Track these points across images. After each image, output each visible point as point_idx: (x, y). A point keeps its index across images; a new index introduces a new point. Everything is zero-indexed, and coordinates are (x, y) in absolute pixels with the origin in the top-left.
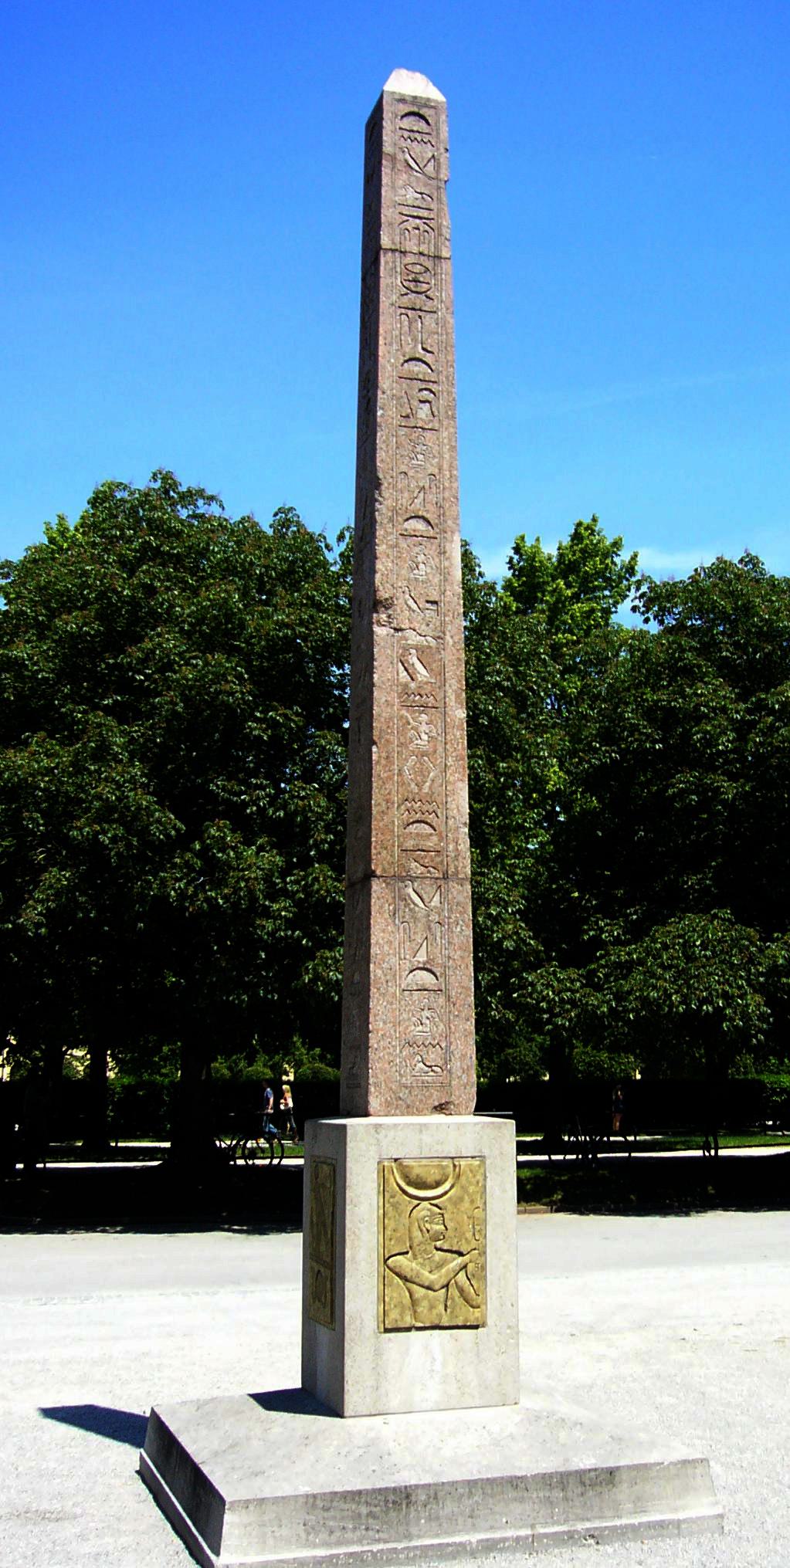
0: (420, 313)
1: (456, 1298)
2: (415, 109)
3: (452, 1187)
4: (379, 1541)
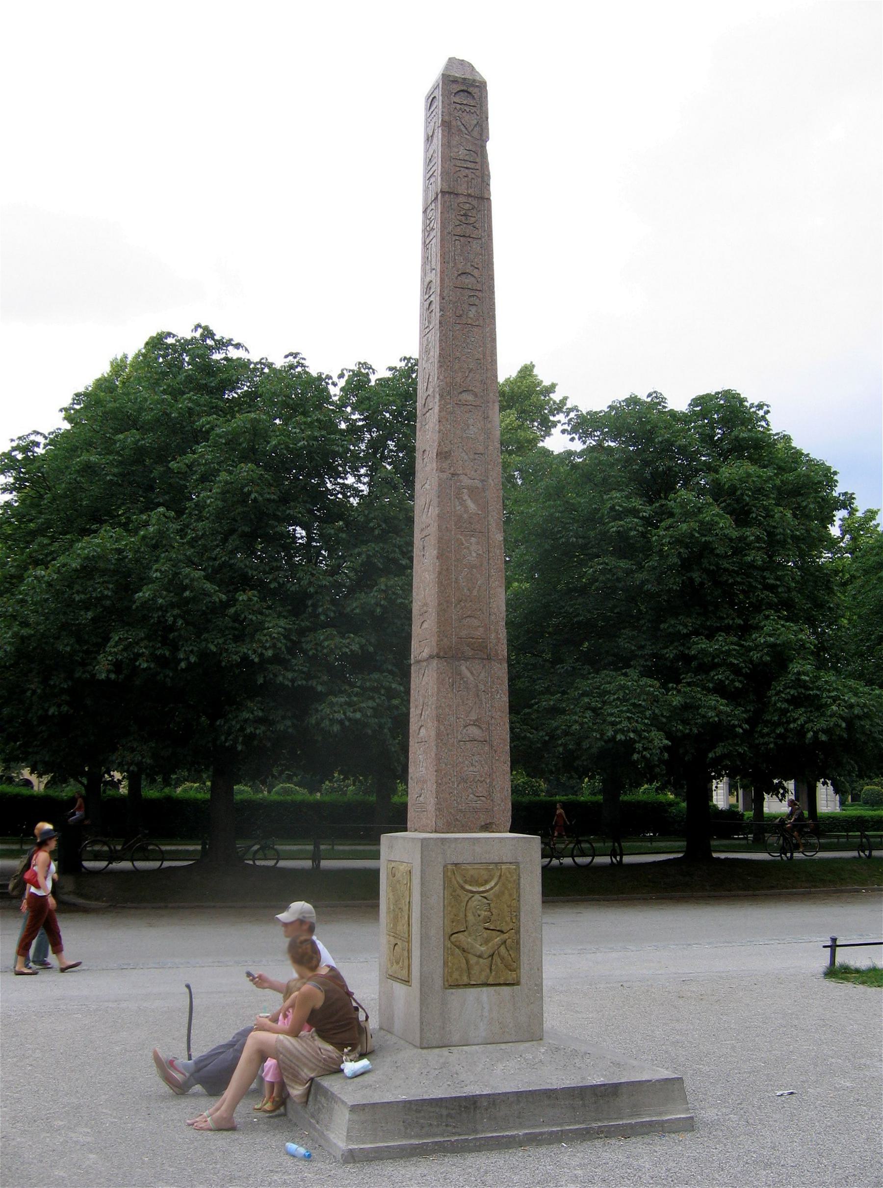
0: (469, 240)
1: (499, 964)
2: (465, 88)
3: (496, 884)
4: (454, 1134)
